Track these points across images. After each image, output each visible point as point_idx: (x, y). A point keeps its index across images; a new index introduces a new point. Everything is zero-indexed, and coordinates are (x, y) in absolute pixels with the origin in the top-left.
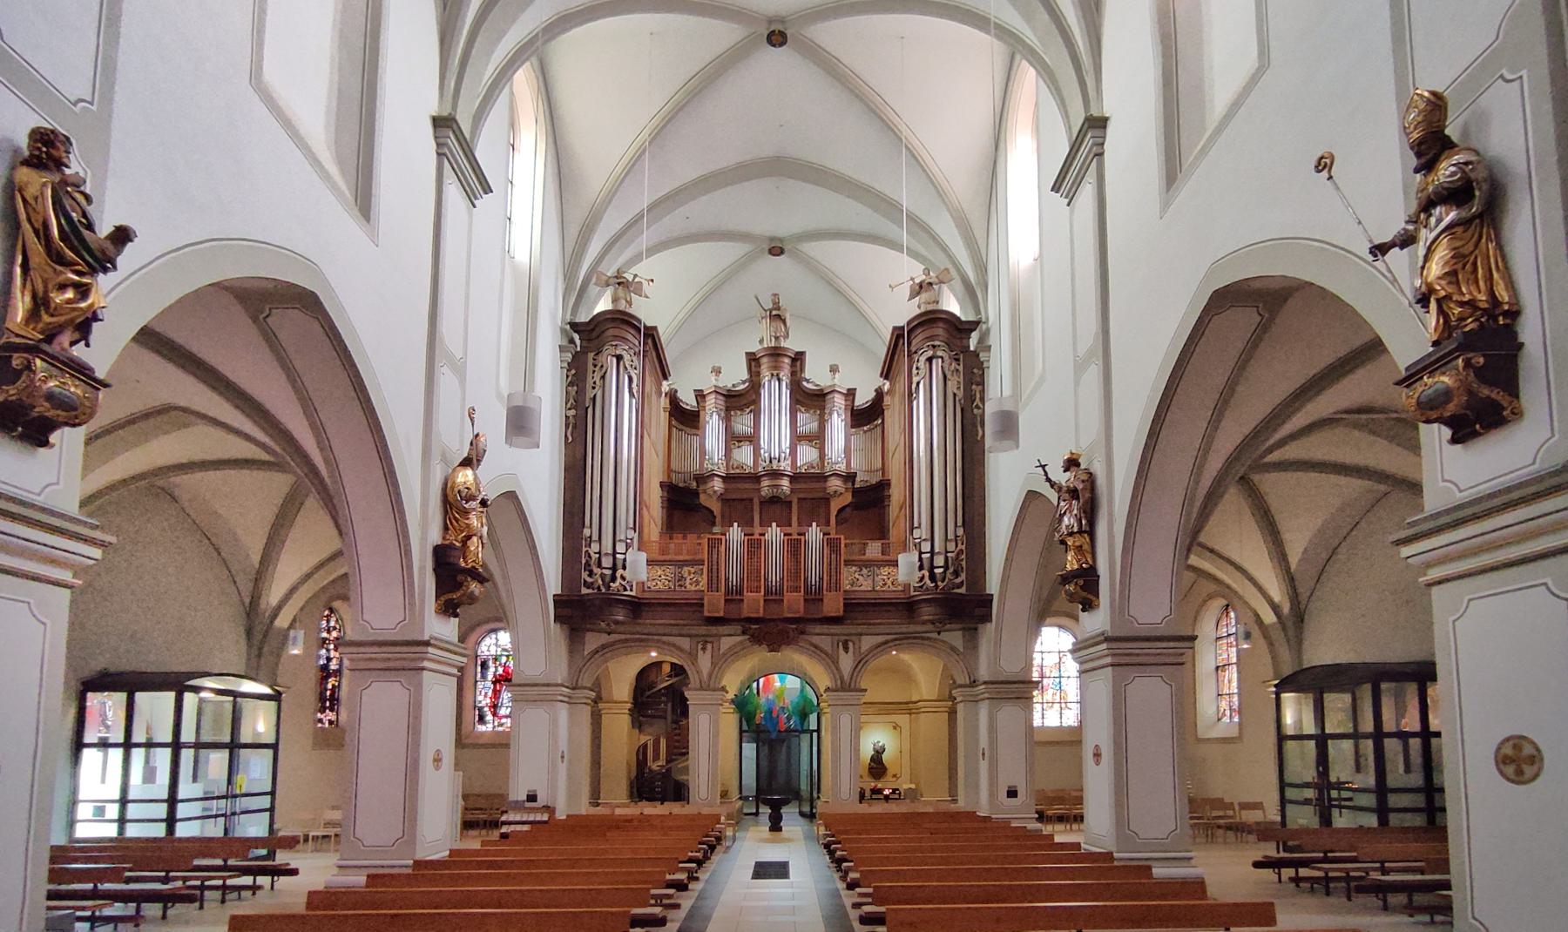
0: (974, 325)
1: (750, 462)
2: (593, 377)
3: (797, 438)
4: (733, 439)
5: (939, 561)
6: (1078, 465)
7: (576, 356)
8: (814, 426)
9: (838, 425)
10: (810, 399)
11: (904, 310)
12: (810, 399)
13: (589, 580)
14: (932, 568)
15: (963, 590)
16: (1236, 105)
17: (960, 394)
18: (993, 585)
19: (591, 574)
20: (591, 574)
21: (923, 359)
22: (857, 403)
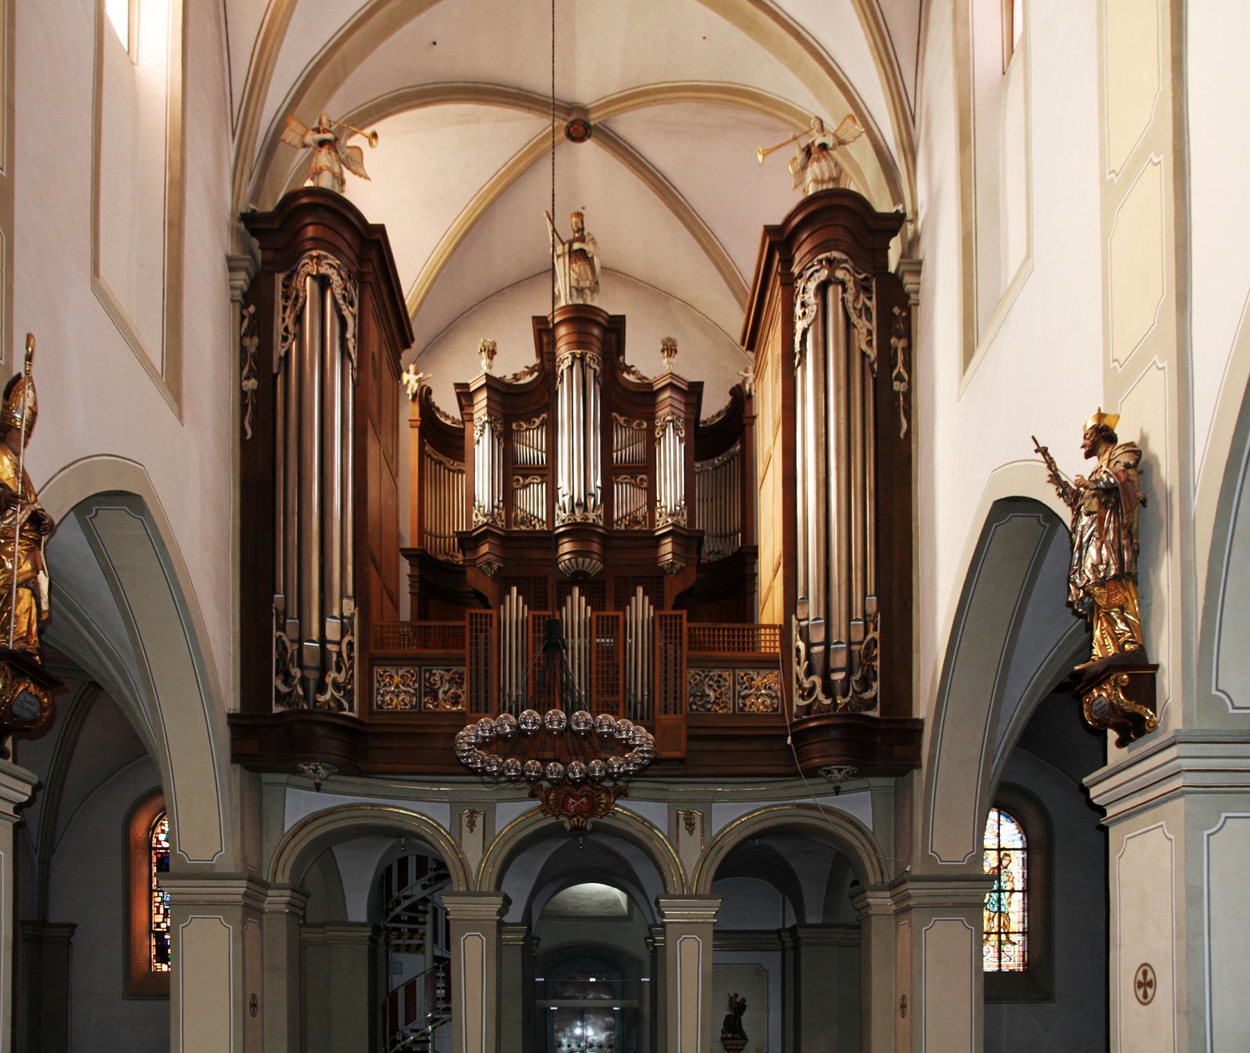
0: (895, 222)
1: (542, 513)
2: (282, 321)
3: (611, 472)
4: (512, 472)
5: (839, 660)
6: (1111, 439)
7: (254, 282)
8: (639, 449)
9: (671, 454)
10: (625, 402)
11: (779, 203)
12: (625, 402)
13: (284, 689)
14: (827, 672)
15: (875, 713)
16: (1020, 270)
17: (873, 354)
18: (923, 708)
19: (287, 679)
20: (287, 679)
21: (812, 286)
22: (703, 417)
